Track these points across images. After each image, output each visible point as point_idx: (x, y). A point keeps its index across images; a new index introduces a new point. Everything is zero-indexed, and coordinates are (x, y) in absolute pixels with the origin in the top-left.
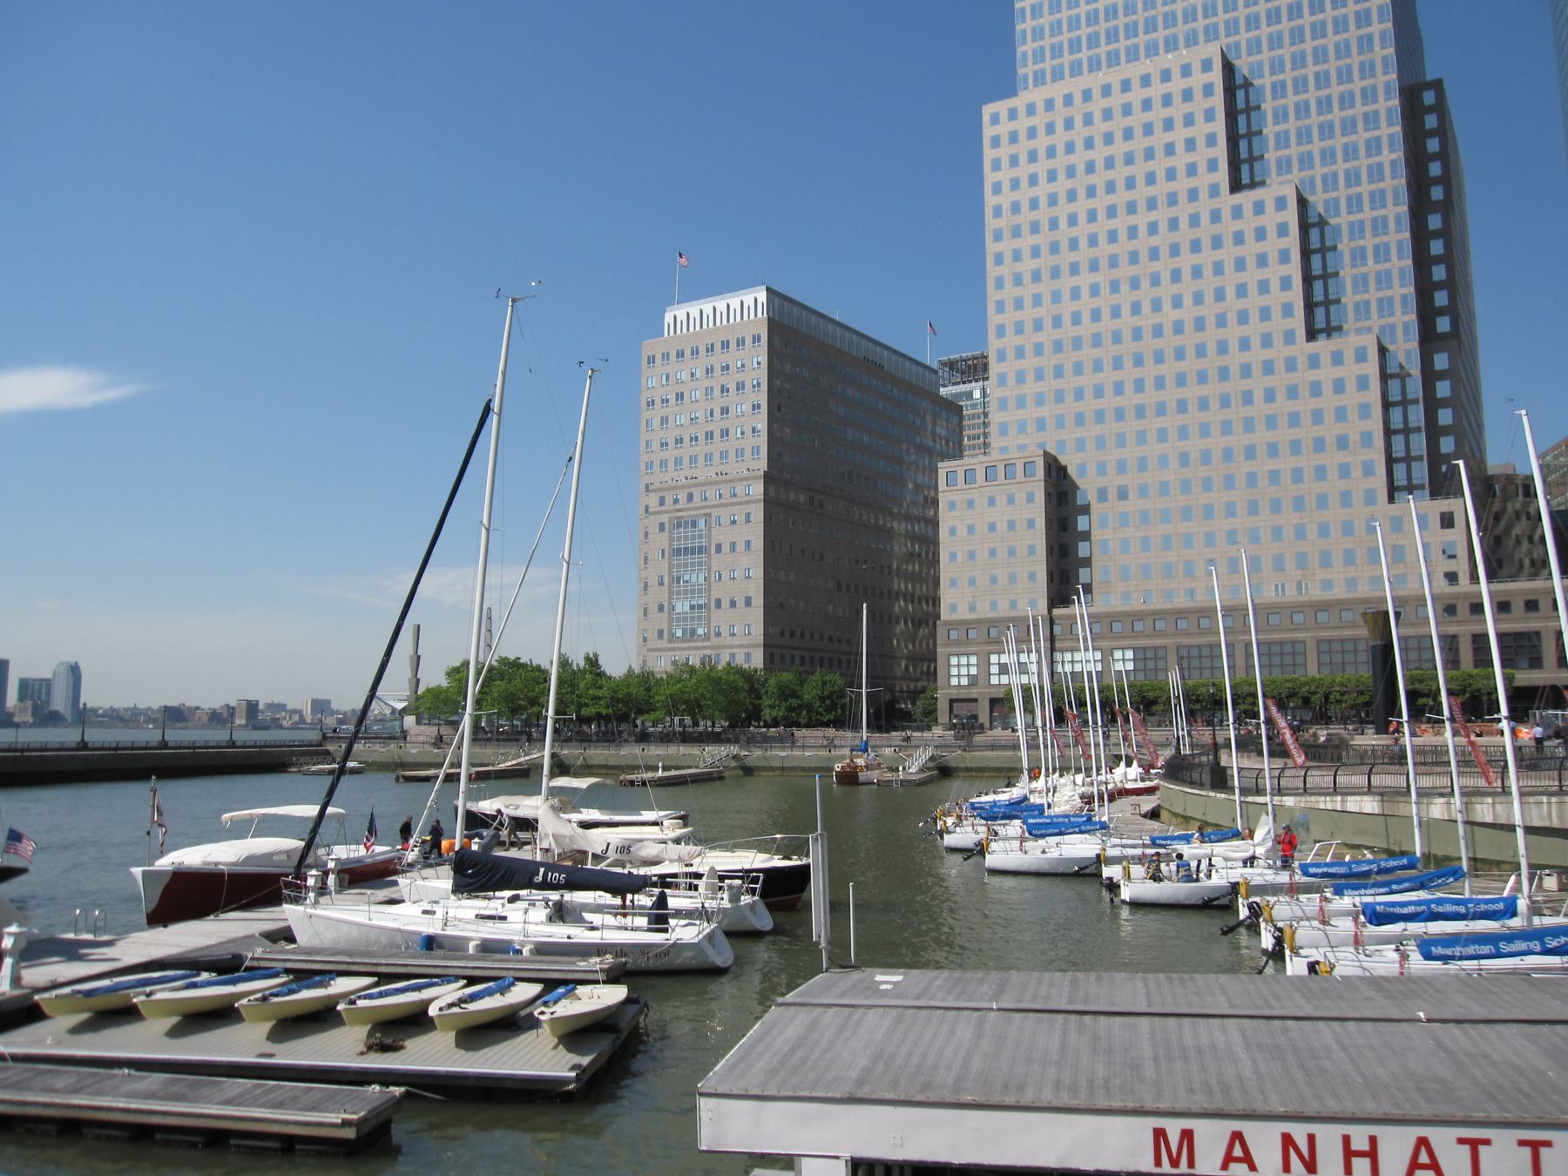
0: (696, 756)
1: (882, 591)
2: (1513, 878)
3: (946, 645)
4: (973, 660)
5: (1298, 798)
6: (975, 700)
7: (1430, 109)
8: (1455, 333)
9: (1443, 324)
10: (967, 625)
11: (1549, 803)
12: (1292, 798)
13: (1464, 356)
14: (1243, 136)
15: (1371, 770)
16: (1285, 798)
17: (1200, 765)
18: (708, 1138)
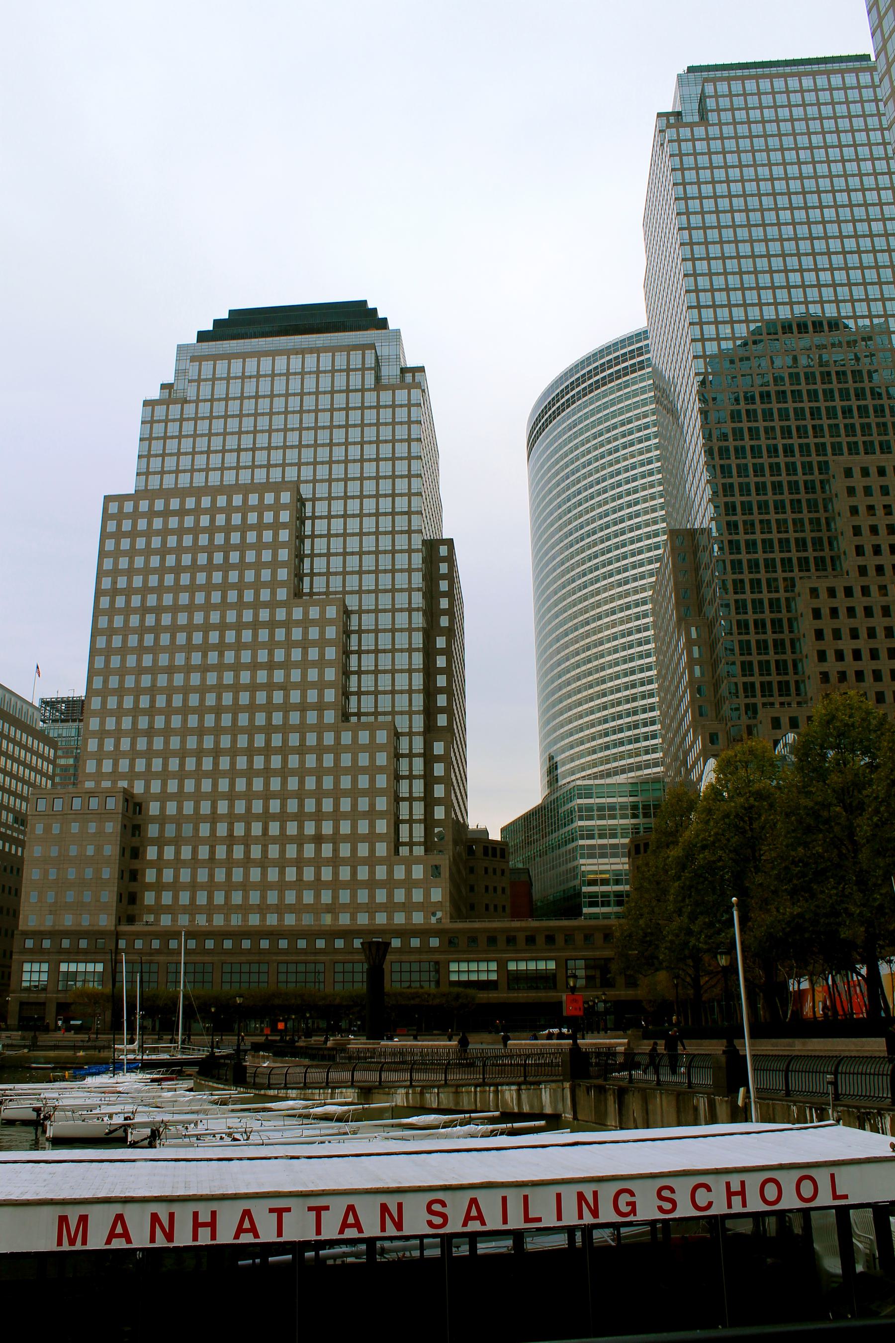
0: (622, 1079)
1: (8, 910)
2: (742, 1090)
3: (21, 953)
4: (45, 967)
5: (299, 1091)
6: (44, 1004)
7: (444, 577)
8: (449, 728)
9: (442, 720)
10: (39, 935)
11: (475, 1092)
12: (294, 1091)
13: (455, 746)
14: (308, 556)
15: (382, 1067)
16: (290, 1091)
17: (225, 1065)
18: (882, 1041)
